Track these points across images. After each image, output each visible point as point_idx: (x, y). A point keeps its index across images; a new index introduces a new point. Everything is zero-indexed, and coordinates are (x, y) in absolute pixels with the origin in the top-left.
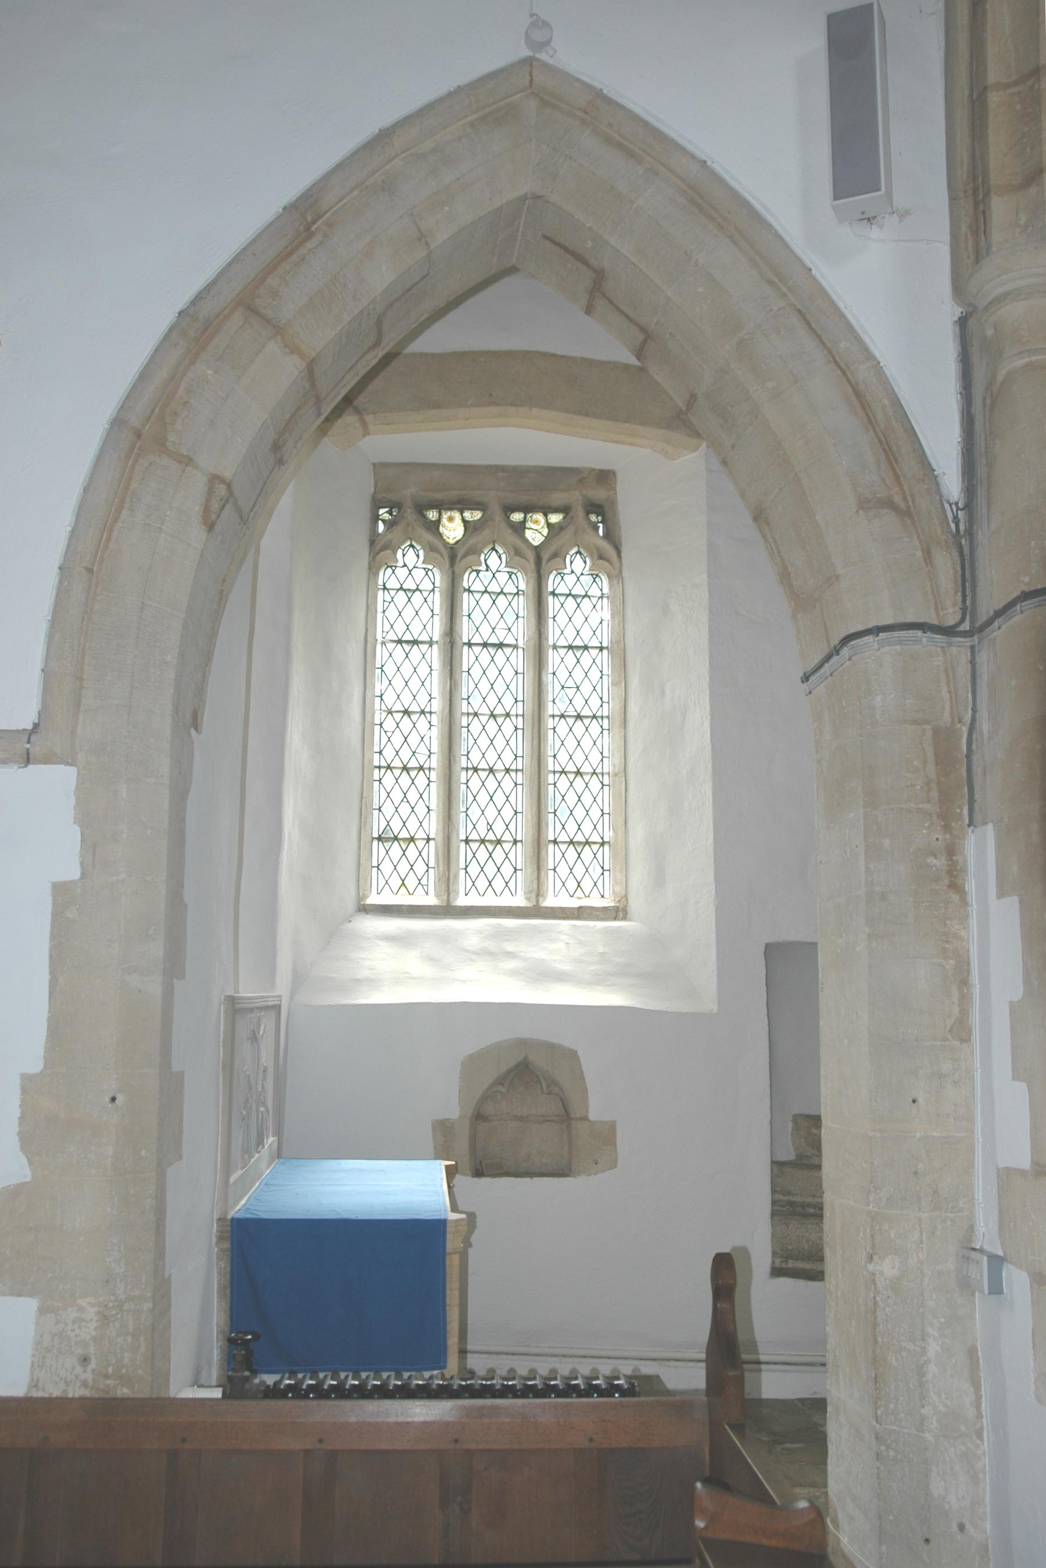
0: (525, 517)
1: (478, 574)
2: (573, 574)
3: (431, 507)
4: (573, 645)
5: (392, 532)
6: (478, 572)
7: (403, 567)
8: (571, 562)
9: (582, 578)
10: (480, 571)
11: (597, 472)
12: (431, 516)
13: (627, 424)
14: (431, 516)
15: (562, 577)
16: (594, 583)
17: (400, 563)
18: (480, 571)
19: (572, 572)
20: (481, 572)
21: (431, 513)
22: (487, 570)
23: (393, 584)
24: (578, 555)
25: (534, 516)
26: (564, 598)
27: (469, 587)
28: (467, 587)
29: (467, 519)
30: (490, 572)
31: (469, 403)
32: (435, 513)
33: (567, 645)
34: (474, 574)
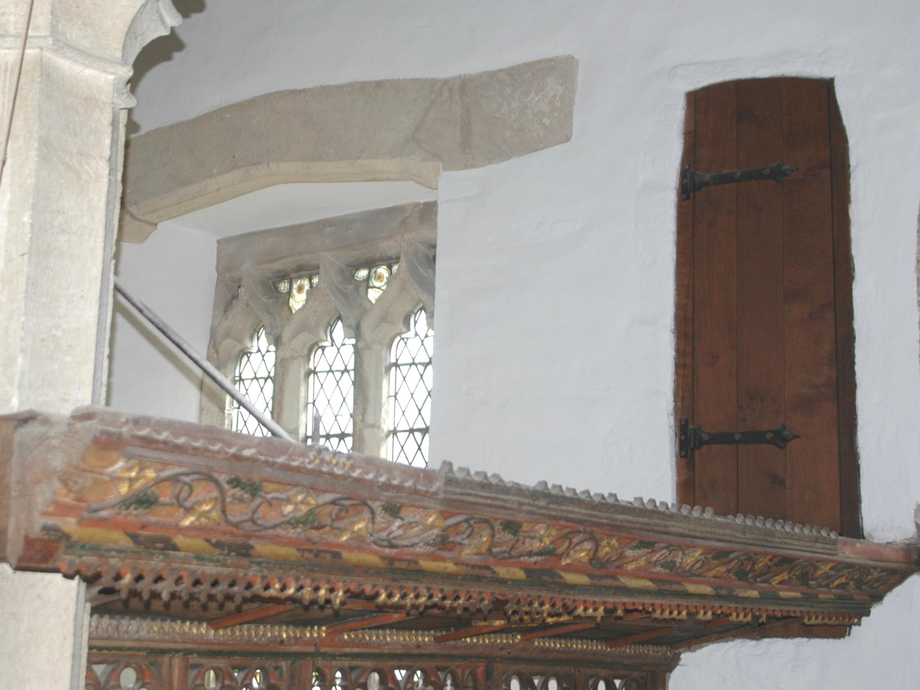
0: (369, 273)
1: (323, 351)
2: (259, 353)
3: (358, 268)
4: (415, 427)
5: (227, 318)
6: (323, 348)
7: (257, 352)
8: (416, 322)
9: (342, 349)
10: (325, 347)
11: (421, 206)
12: (282, 289)
13: (360, 160)
14: (282, 289)
15: (406, 343)
16: (323, 355)
17: (255, 349)
18: (325, 347)
19: (416, 335)
20: (252, 354)
21: (283, 284)
22: (332, 345)
23: (322, 366)
24: (423, 311)
25: (378, 270)
26: (340, 374)
27: (315, 368)
28: (313, 369)
29: (431, 270)
30: (335, 346)
31: (214, 171)
32: (286, 283)
33: (408, 428)
34: (320, 350)
